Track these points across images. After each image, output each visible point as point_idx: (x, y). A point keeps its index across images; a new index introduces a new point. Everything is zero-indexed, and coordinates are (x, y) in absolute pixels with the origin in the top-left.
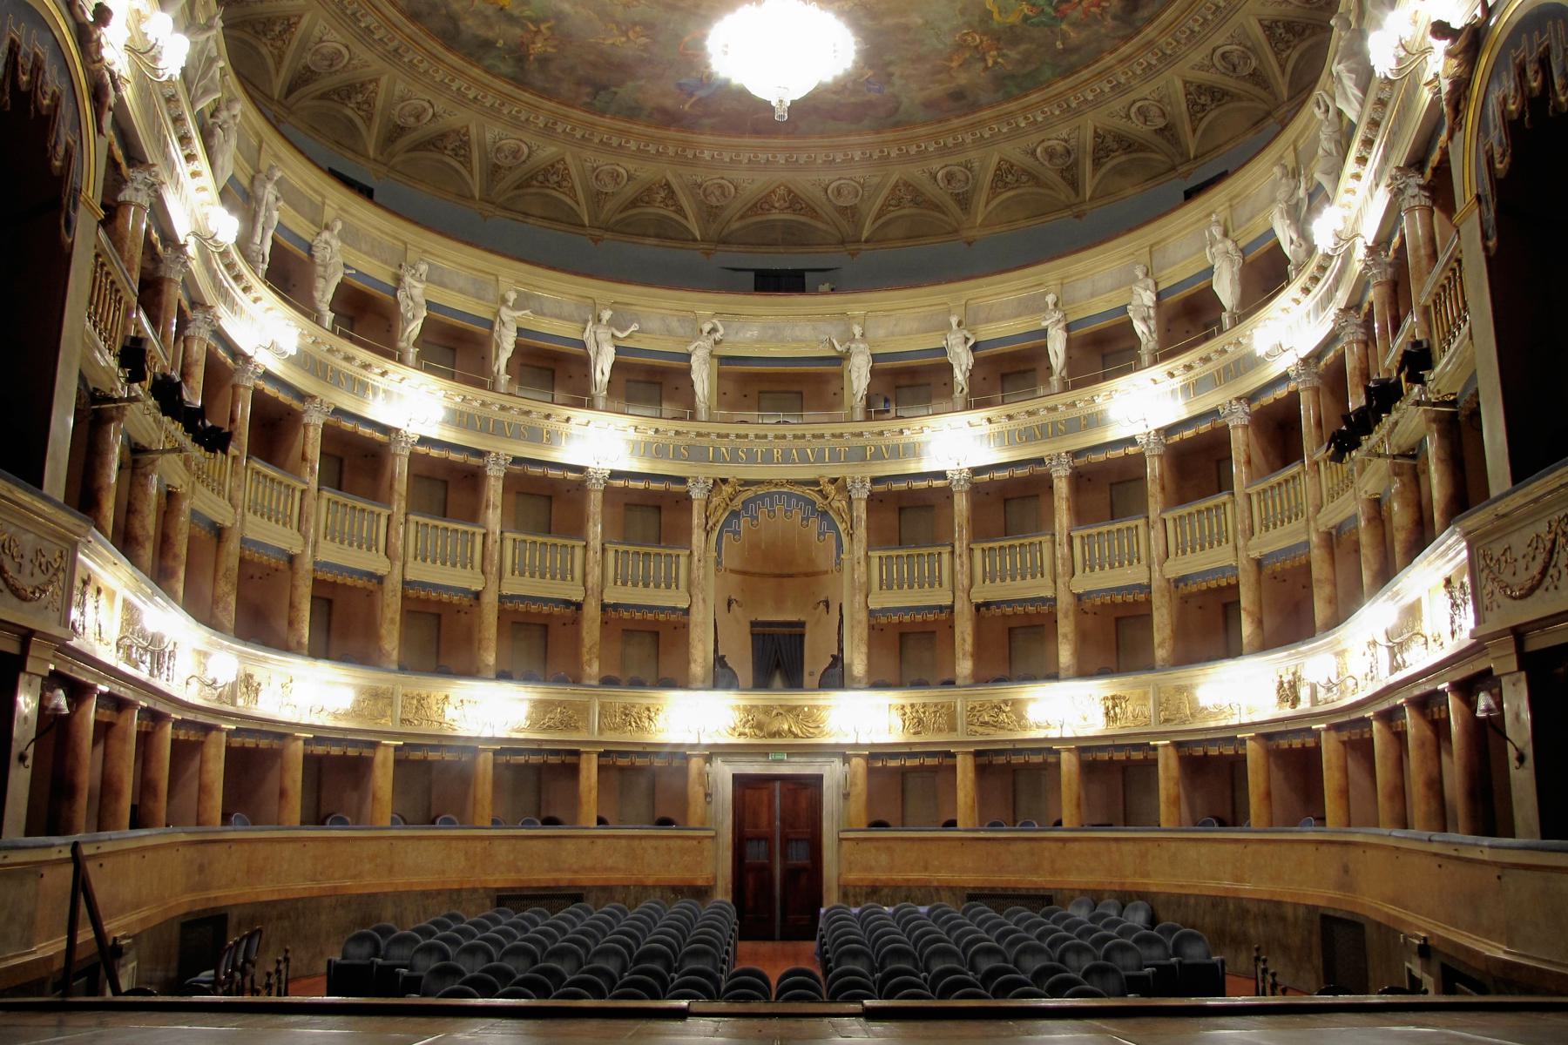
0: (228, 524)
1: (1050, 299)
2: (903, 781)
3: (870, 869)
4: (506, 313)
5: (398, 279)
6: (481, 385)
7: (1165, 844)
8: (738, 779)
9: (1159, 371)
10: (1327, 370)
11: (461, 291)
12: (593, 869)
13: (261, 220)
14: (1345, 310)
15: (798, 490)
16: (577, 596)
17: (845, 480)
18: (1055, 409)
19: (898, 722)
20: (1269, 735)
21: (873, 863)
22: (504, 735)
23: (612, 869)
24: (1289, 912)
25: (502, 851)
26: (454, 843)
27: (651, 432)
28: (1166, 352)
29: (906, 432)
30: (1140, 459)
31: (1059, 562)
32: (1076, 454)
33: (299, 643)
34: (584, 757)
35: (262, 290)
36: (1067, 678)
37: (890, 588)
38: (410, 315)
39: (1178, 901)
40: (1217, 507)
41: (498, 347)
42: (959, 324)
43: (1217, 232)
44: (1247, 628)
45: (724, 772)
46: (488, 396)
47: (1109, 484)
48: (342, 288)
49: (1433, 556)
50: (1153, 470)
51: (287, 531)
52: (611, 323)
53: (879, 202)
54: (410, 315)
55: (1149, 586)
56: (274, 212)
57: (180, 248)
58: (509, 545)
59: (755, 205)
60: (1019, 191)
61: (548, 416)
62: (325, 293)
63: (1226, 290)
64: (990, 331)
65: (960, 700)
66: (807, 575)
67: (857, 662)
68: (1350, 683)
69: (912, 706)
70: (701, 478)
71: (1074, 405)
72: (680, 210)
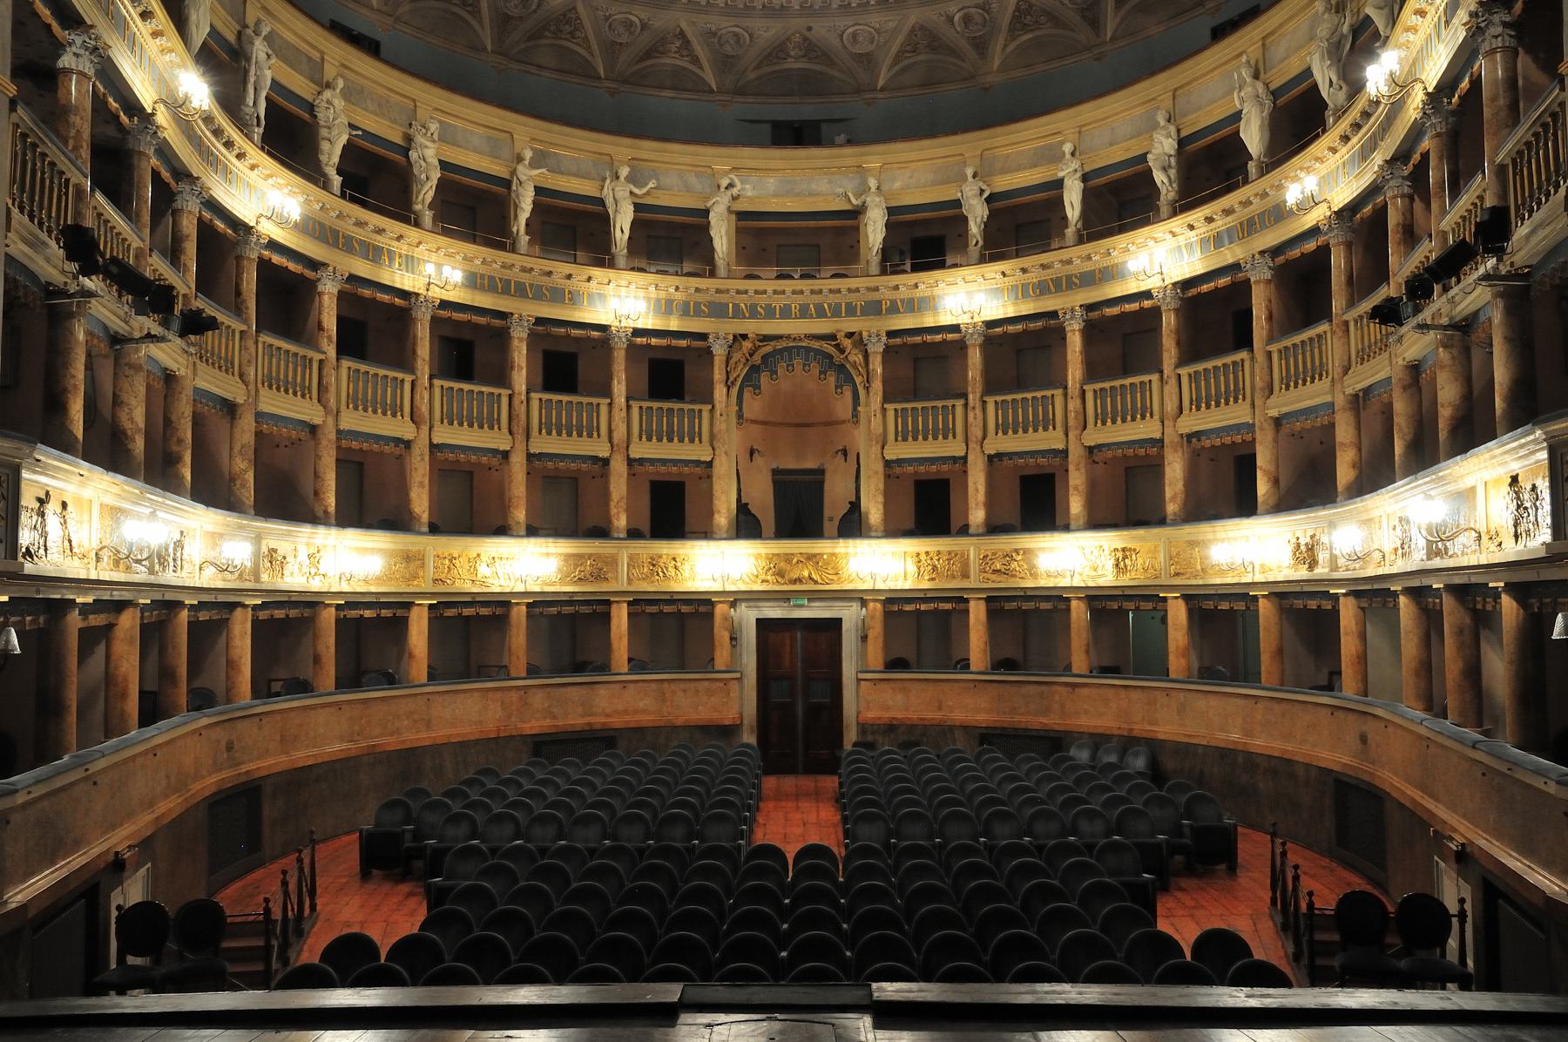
0: (240, 400)
1: (1068, 148)
2: (919, 627)
3: (888, 708)
4: (524, 172)
5: (409, 139)
6: (501, 246)
7: (1173, 694)
8: (761, 623)
9: (1178, 223)
10: (1364, 223)
11: (475, 150)
12: (626, 712)
13: (252, 80)
14: (1391, 162)
15: (816, 345)
16: (603, 451)
17: (861, 334)
18: (1070, 262)
19: (912, 568)
20: (1284, 596)
21: (890, 703)
22: (537, 589)
23: (643, 711)
24: (1301, 772)
25: (538, 700)
26: (490, 695)
27: (672, 290)
28: (1183, 205)
29: (922, 287)
30: (1156, 312)
31: (1072, 415)
32: (1090, 308)
33: (326, 512)
34: (614, 608)
35: (255, 155)
36: (1078, 530)
37: (905, 439)
38: (423, 176)
39: (1184, 750)
40: (1234, 363)
41: (516, 206)
42: (974, 176)
43: (1246, 74)
44: (1263, 487)
45: (748, 616)
47: (1123, 336)
48: (348, 149)
49: (1498, 451)
50: (1169, 324)
51: (306, 403)
52: (631, 179)
53: (894, 50)
54: (423, 176)
55: (1161, 441)
56: (265, 69)
57: (147, 118)
58: (535, 405)
59: (770, 54)
60: (1038, 33)
61: (569, 277)
62: (331, 153)
63: (1253, 137)
64: (1004, 183)
65: (971, 548)
67: (874, 511)
68: (1377, 555)
70: (722, 334)
71: (1089, 258)
72: (696, 60)
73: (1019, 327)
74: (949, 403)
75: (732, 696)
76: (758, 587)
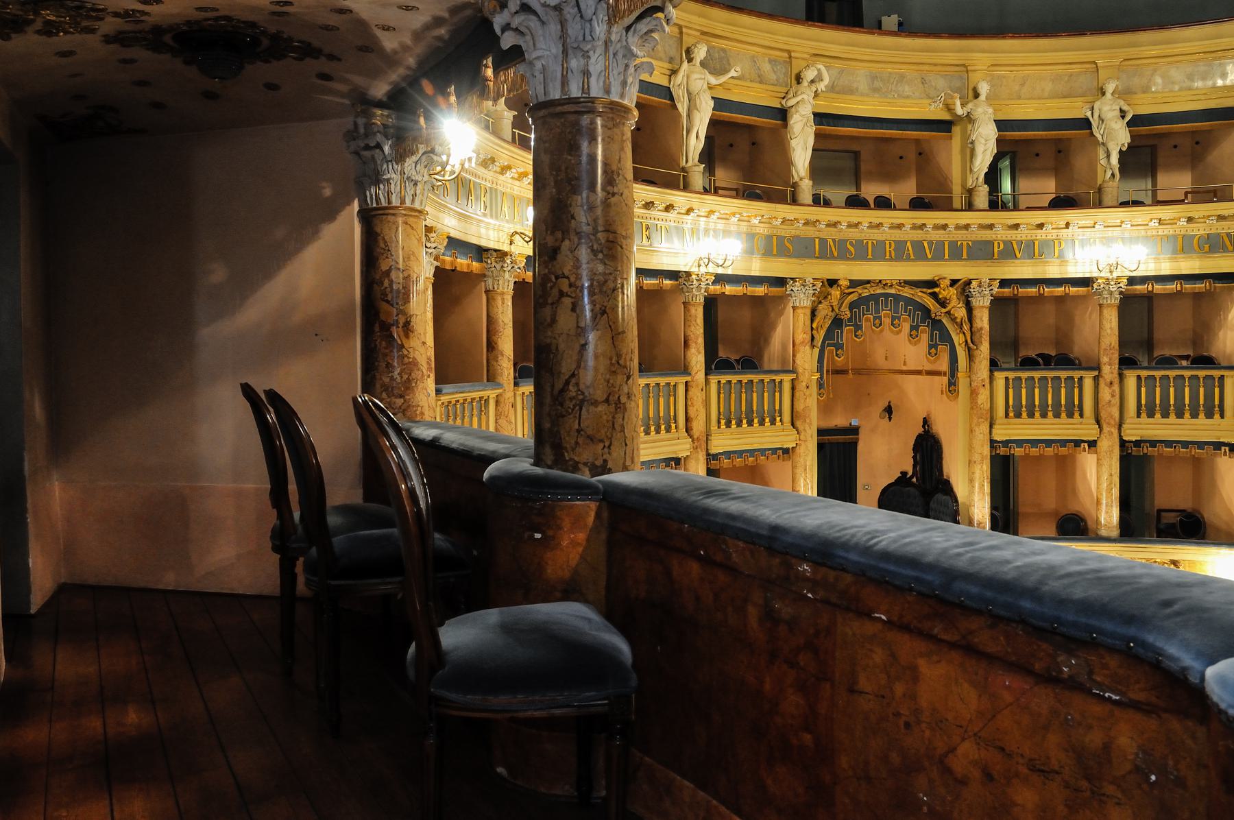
15: (907, 292)
27: (755, 221)
29: (1048, 227)
37: (1018, 415)
46: (783, 211)
73: (1171, 287)
74: (1076, 374)
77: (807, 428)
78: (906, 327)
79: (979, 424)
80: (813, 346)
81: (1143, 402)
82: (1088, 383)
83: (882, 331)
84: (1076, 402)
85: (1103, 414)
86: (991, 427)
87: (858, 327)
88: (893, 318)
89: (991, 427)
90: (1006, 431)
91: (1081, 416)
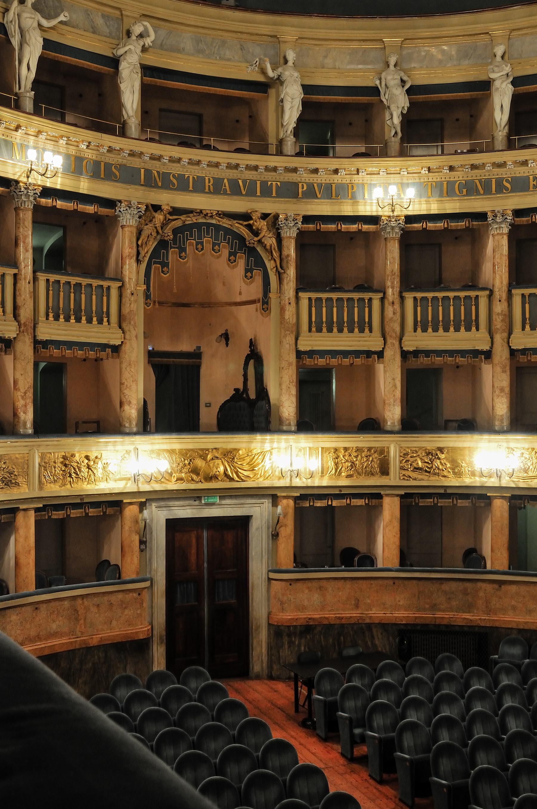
2: (324, 526)
3: (303, 608)
15: (226, 223)
17: (276, 217)
18: (502, 165)
21: (306, 603)
27: (83, 146)
29: (342, 173)
34: (20, 516)
37: (319, 330)
45: (158, 516)
64: (423, 77)
66: (202, 305)
69: (346, 449)
70: (134, 202)
73: (440, 225)
75: (137, 608)
76: (172, 486)
77: (132, 329)
78: (225, 252)
79: (285, 336)
80: (138, 261)
81: (419, 319)
82: (376, 304)
83: (203, 255)
84: (367, 320)
85: (387, 329)
86: (297, 339)
87: (182, 250)
88: (214, 245)
89: (297, 339)
90: (310, 342)
91: (371, 331)
